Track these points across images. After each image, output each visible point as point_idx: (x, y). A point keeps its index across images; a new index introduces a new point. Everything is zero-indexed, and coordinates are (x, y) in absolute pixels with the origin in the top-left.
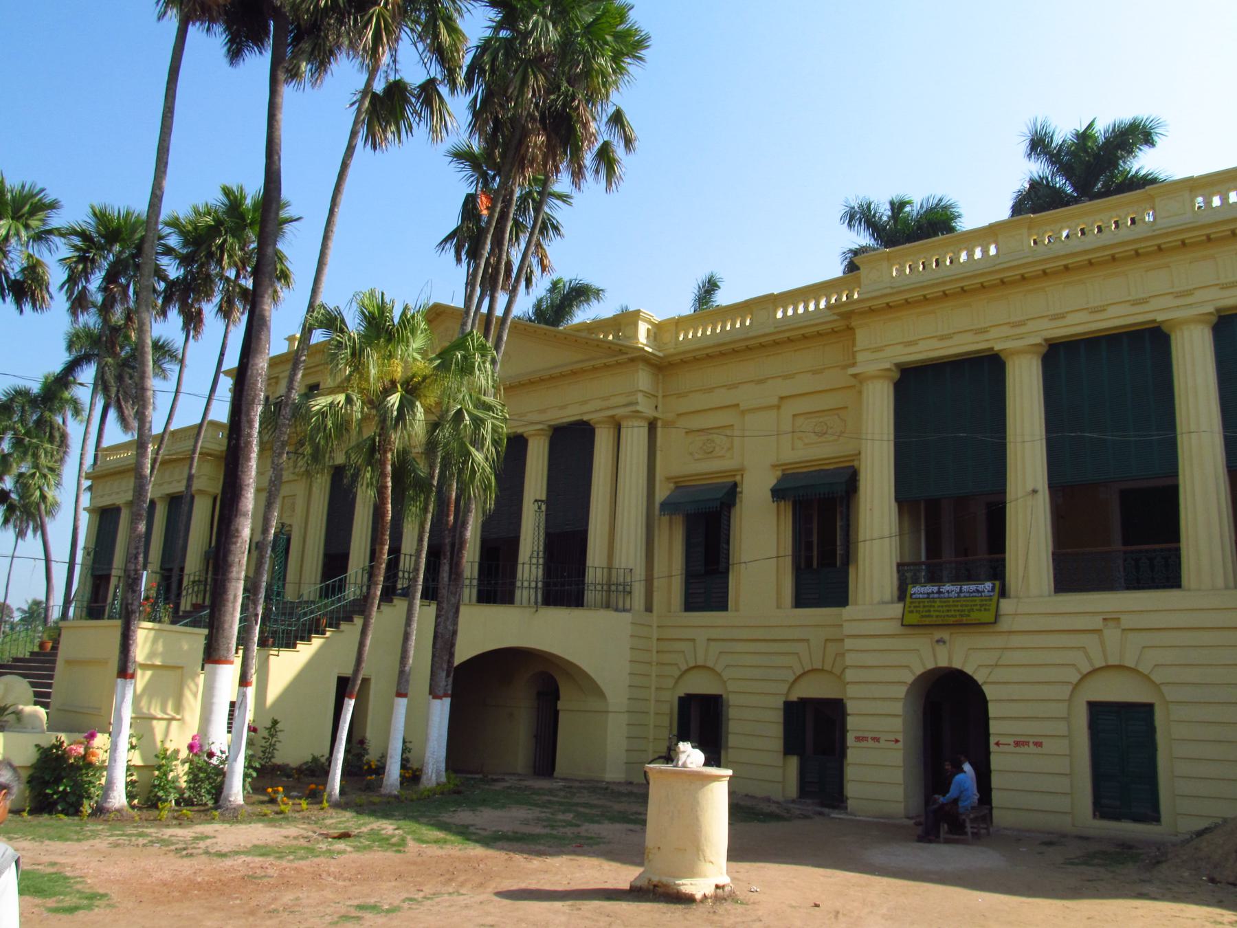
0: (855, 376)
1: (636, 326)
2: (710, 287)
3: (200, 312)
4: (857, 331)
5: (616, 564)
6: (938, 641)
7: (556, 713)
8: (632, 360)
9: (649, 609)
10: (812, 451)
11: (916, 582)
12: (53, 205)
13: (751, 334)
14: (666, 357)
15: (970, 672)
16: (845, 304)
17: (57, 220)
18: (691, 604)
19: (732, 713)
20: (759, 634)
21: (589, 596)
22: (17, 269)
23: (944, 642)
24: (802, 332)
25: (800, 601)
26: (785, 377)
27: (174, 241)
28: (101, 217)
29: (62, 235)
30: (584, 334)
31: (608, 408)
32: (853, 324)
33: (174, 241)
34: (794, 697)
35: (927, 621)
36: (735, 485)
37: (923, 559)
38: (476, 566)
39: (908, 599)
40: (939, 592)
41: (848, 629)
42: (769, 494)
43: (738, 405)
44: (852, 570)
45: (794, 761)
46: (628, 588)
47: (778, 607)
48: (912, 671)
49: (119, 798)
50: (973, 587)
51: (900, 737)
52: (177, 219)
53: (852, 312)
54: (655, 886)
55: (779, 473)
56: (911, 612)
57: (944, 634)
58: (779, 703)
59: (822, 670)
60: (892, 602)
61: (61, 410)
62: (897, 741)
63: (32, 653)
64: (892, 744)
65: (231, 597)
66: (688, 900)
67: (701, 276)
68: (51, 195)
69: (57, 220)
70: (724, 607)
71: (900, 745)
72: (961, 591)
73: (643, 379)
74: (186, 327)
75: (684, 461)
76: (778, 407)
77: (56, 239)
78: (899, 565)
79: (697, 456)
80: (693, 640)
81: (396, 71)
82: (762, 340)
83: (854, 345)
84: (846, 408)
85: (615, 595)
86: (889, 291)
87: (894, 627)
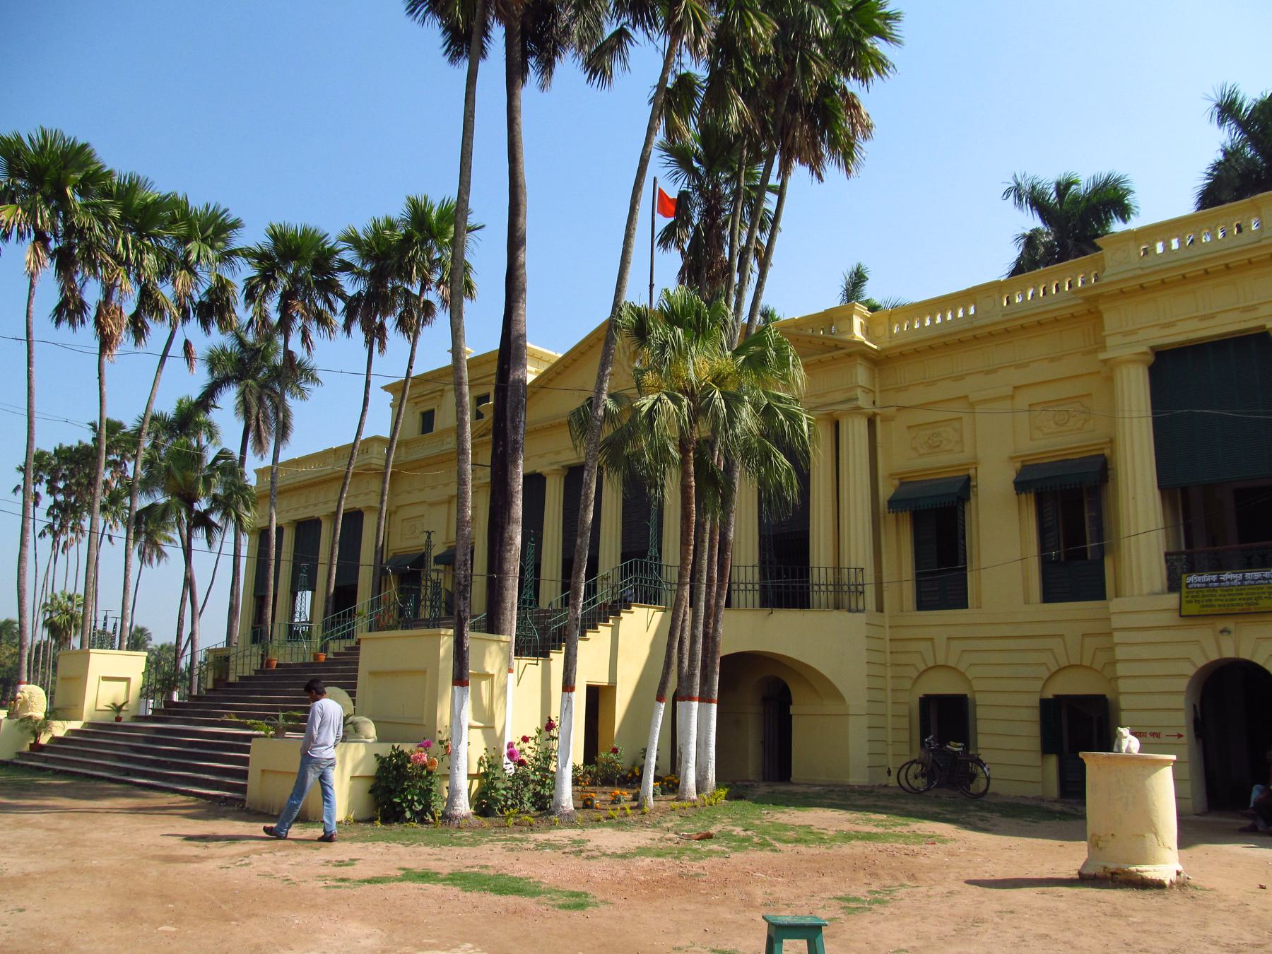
0: (1105, 361)
1: (850, 320)
2: (857, 281)
3: (382, 327)
4: (1105, 315)
5: (844, 563)
6: (1222, 632)
7: (789, 718)
8: (849, 355)
9: (880, 609)
10: (1055, 439)
11: (1192, 570)
12: (236, 225)
13: (976, 323)
14: (883, 350)
15: (1261, 663)
16: (1095, 287)
17: (241, 240)
18: (925, 602)
19: (980, 712)
20: (1007, 631)
21: (814, 597)
22: (202, 291)
23: (1229, 632)
24: (1037, 318)
25: (1049, 596)
26: (1018, 366)
27: (349, 256)
28: (278, 237)
29: (245, 256)
30: (793, 330)
31: (826, 405)
32: (1101, 307)
33: (349, 256)
34: (1049, 695)
35: (1209, 611)
36: (969, 478)
37: (1183, 548)
38: (757, 570)
39: (1184, 590)
40: (1219, 581)
41: (1116, 622)
42: (1012, 486)
43: (966, 397)
44: (1108, 563)
45: (1053, 761)
46: (860, 588)
47: (1027, 602)
48: (1193, 664)
49: (463, 807)
50: (1258, 575)
51: (1183, 732)
52: (354, 232)
53: (1101, 295)
54: (1113, 874)
55: (1018, 465)
56: (1190, 602)
57: (1229, 624)
58: (1035, 700)
59: (1081, 666)
60: (1163, 593)
61: (196, 433)
62: (1180, 736)
63: (256, 671)
64: (1175, 740)
65: (509, 605)
66: (1159, 885)
67: (848, 268)
68: (234, 215)
69: (241, 240)
70: (964, 605)
71: (1184, 740)
72: (1244, 579)
73: (861, 374)
74: (369, 343)
75: (907, 456)
76: (1012, 397)
77: (239, 261)
78: (1166, 554)
79: (922, 451)
80: (932, 639)
81: (681, 65)
82: (992, 329)
83: (1103, 329)
84: (1090, 395)
85: (843, 596)
86: (1139, 272)
87: (1170, 618)
